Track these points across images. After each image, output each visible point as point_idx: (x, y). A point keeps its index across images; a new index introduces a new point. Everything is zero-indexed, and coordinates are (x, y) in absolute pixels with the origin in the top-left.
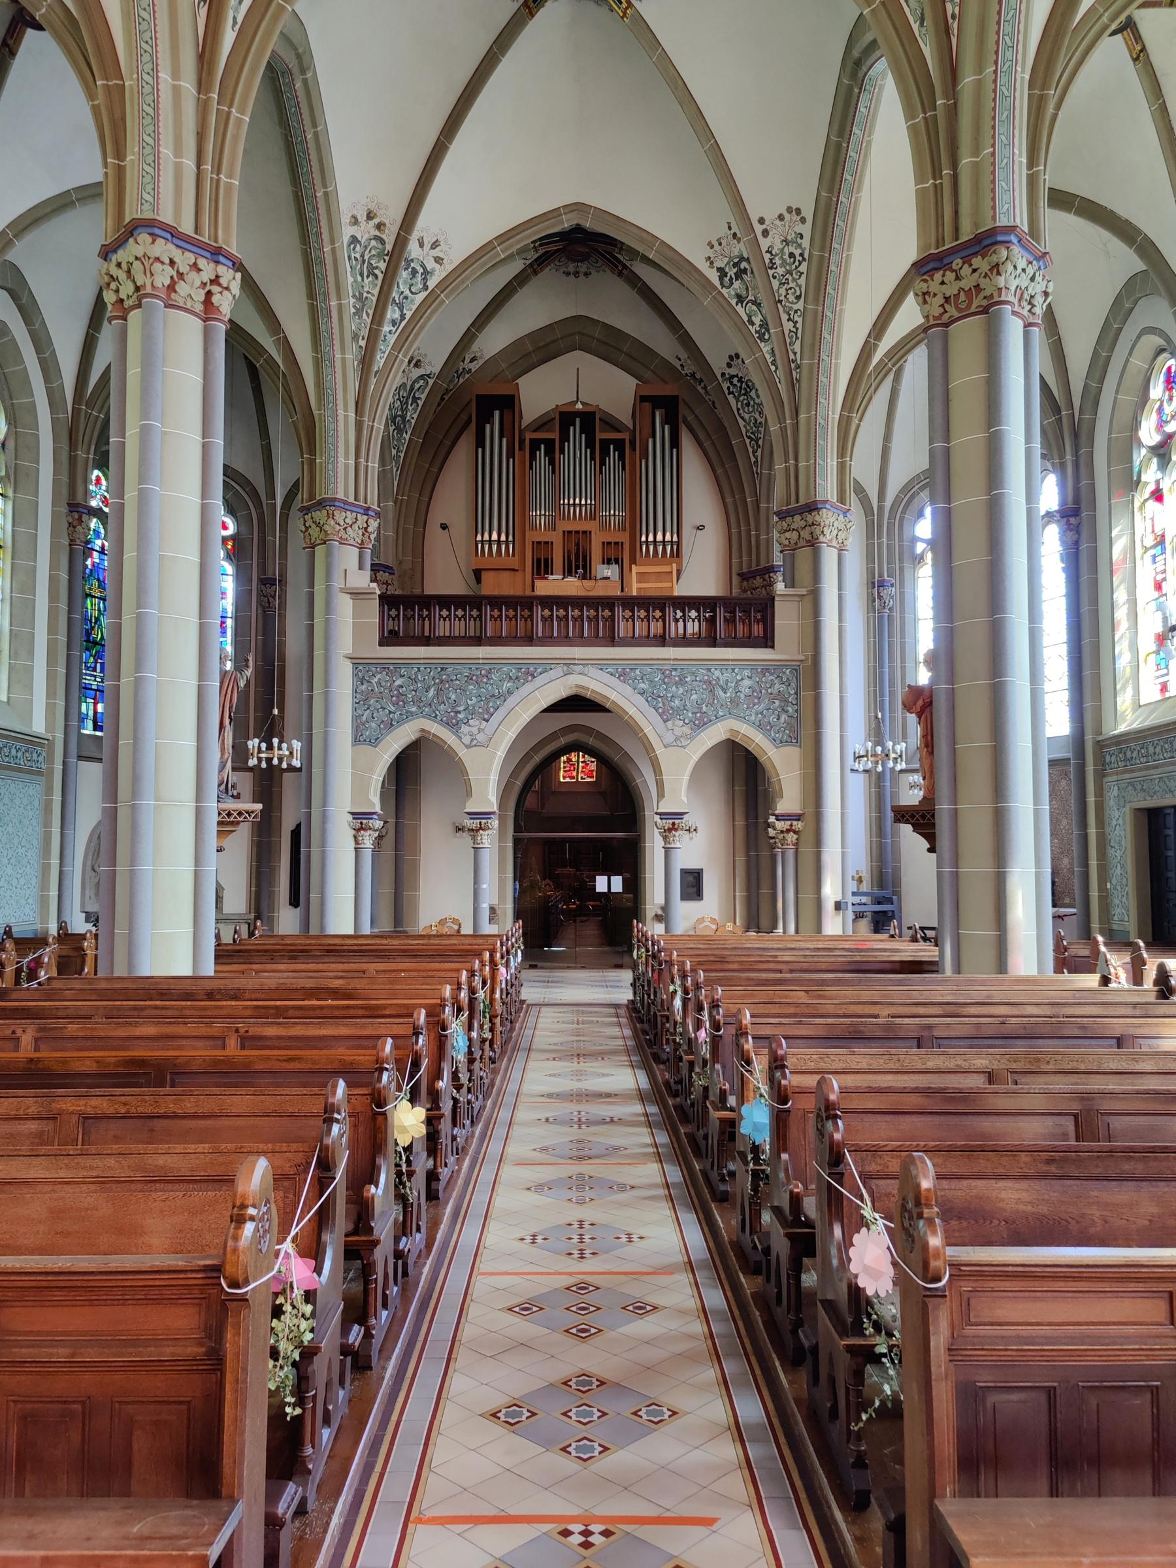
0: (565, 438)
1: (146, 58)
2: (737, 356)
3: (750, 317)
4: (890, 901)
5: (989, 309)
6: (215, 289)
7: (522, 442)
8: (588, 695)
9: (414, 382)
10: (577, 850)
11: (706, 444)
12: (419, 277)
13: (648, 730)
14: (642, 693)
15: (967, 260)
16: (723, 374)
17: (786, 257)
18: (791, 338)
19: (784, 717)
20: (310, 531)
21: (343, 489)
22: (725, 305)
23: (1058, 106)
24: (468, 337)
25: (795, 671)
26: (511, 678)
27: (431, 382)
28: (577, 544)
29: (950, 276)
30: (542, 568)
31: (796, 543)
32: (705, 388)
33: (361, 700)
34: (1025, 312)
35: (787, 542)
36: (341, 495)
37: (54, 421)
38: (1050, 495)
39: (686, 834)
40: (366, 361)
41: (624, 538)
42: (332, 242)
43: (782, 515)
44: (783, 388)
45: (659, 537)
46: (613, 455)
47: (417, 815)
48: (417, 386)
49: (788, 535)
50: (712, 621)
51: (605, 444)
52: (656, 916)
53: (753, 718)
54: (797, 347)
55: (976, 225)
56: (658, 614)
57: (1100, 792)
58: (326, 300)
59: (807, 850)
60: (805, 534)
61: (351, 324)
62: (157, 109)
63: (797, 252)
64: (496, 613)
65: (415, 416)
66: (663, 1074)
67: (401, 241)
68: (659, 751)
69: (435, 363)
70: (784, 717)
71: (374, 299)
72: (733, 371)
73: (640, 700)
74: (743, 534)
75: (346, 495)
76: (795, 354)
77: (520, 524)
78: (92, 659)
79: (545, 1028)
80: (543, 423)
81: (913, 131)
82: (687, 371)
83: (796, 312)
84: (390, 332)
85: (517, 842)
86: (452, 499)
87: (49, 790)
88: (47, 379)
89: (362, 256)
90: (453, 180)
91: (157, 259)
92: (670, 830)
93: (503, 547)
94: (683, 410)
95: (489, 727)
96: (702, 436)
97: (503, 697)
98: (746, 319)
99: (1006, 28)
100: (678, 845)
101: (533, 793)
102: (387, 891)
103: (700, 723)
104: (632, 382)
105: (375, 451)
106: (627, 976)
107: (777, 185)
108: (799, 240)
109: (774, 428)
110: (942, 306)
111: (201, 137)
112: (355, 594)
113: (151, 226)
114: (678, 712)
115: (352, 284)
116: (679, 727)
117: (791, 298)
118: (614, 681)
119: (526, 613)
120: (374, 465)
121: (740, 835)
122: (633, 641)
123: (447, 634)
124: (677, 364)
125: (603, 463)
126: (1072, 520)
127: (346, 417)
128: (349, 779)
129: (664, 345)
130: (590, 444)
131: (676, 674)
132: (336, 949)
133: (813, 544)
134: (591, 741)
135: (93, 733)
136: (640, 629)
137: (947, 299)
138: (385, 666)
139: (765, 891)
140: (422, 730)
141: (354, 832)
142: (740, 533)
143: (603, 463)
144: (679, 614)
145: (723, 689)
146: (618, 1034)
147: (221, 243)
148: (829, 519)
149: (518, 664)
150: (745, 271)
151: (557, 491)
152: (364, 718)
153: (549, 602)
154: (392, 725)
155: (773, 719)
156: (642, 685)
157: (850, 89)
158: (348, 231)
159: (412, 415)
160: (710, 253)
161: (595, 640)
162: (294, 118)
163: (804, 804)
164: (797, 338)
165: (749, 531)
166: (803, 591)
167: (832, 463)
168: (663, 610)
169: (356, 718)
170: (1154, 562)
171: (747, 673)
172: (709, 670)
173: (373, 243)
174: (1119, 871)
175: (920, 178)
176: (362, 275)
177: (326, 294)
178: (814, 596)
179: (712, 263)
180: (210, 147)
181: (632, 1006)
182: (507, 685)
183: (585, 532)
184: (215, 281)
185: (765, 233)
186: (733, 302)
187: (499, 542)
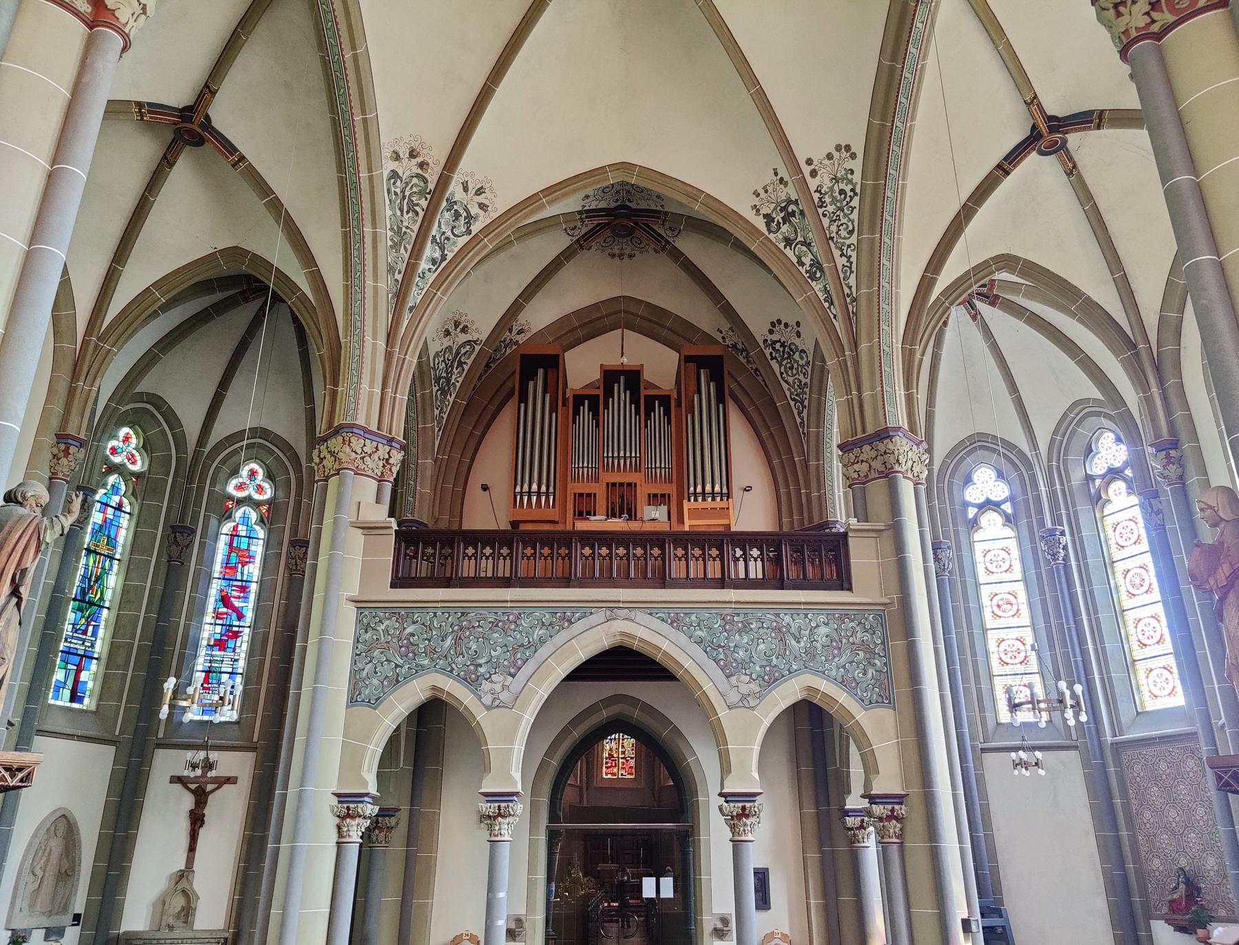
0: (609, 393)
2: (779, 322)
3: (799, 258)
5: (888, 475)
8: (636, 645)
9: (460, 347)
13: (707, 687)
14: (700, 642)
16: (765, 341)
17: (837, 194)
18: (845, 273)
20: (325, 462)
21: (364, 412)
22: (773, 248)
24: (516, 308)
25: (880, 617)
26: (543, 624)
27: (477, 348)
28: (622, 497)
31: (866, 476)
32: (747, 357)
33: (362, 651)
35: (856, 475)
36: (361, 421)
40: (401, 295)
44: (839, 325)
46: (658, 410)
47: (436, 801)
48: (463, 351)
49: (856, 467)
50: (778, 561)
52: (715, 929)
53: (834, 673)
54: (852, 281)
56: (714, 552)
58: (360, 225)
61: (386, 256)
63: (848, 188)
65: (461, 380)
67: (444, 181)
68: (722, 713)
69: (483, 328)
70: (871, 671)
71: (414, 235)
72: (775, 337)
73: (697, 651)
74: (792, 493)
76: (850, 288)
78: (83, 621)
83: (849, 246)
84: (429, 270)
85: (552, 836)
86: (495, 460)
89: (403, 191)
90: (492, 93)
92: (739, 816)
93: (543, 498)
94: (727, 366)
96: (745, 401)
97: (534, 647)
98: (795, 260)
100: (750, 837)
103: (770, 680)
105: (405, 384)
107: (825, 121)
108: (850, 176)
110: (1147, 14)
112: (369, 529)
114: (743, 665)
115: (388, 217)
116: (747, 685)
117: (843, 233)
118: (666, 628)
119: (563, 551)
120: (403, 397)
121: (811, 825)
123: (472, 575)
124: (719, 337)
125: (648, 417)
126: (1173, 453)
127: (374, 345)
129: (703, 317)
130: (635, 400)
135: (68, 704)
136: (695, 569)
139: (846, 898)
140: (434, 688)
141: (337, 820)
142: (789, 494)
143: (648, 417)
144: (739, 553)
145: (795, 638)
150: (793, 214)
152: (364, 673)
154: (398, 682)
155: (858, 674)
156: (699, 633)
160: (757, 201)
161: (643, 581)
162: (330, 34)
164: (852, 272)
168: (720, 549)
169: (354, 673)
171: (822, 618)
172: (778, 615)
173: (415, 180)
176: (401, 210)
177: (360, 221)
179: (758, 211)
182: (539, 632)
183: (629, 484)
185: (814, 174)
186: (781, 246)
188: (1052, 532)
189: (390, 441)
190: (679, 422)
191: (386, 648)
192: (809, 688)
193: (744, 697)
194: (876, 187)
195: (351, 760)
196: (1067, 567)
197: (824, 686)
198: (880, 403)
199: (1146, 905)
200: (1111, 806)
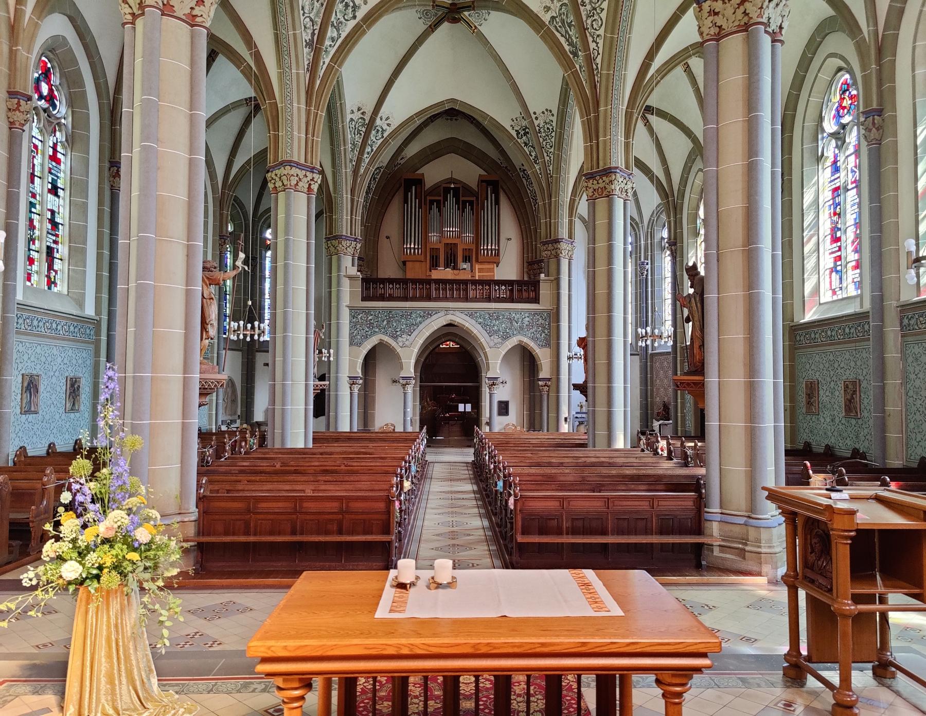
0: (446, 199)
5: (609, 196)
10: (450, 378)
13: (482, 340)
21: (345, 230)
24: (400, 150)
25: (549, 315)
29: (595, 182)
30: (434, 265)
33: (353, 325)
36: (344, 233)
39: (501, 384)
40: (356, 172)
41: (473, 247)
43: (544, 243)
50: (512, 291)
51: (464, 202)
54: (599, 60)
55: (605, 164)
58: (339, 145)
59: (552, 394)
61: (349, 156)
66: (482, 485)
79: (437, 471)
80: (436, 187)
86: (391, 224)
95: (411, 338)
97: (417, 325)
99: (615, 92)
103: (506, 337)
106: (472, 450)
112: (351, 278)
113: (290, 163)
115: (351, 137)
116: (496, 339)
118: (467, 318)
121: (527, 385)
122: (475, 300)
125: (463, 211)
128: (349, 362)
130: (457, 202)
131: (495, 316)
132: (348, 438)
133: (557, 257)
138: (367, 311)
146: (466, 473)
149: (424, 310)
153: (438, 282)
155: (538, 336)
163: (552, 374)
166: (552, 278)
169: (351, 334)
175: (585, 142)
178: (558, 281)
180: (311, 128)
181: (473, 463)
182: (419, 319)
184: (312, 180)
185: (537, 118)
187: (414, 248)
188: (643, 264)
190: (477, 213)
191: (362, 324)
195: (352, 365)
196: (647, 279)
198: (607, 150)
199: (652, 414)
200: (646, 377)
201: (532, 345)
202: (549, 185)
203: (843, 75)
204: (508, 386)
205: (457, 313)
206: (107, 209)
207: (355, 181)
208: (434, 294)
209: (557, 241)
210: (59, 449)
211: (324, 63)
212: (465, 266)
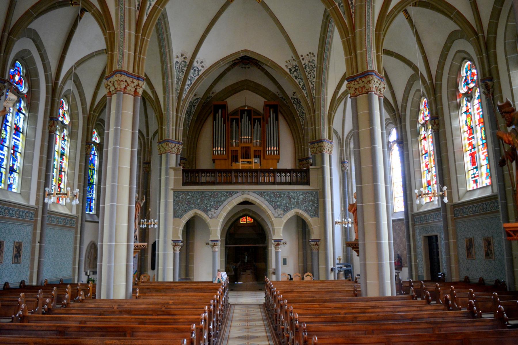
1: (122, 26)
4: (350, 266)
5: (368, 92)
6: (138, 87)
7: (228, 118)
10: (247, 251)
11: (287, 119)
12: (197, 72)
13: (269, 212)
14: (267, 200)
15: (360, 79)
19: (313, 208)
23: (384, 36)
29: (356, 83)
30: (235, 159)
34: (378, 93)
36: (171, 138)
37: (83, 117)
38: (394, 136)
40: (179, 97)
42: (170, 63)
43: (312, 143)
45: (272, 149)
51: (255, 120)
54: (314, 92)
55: (363, 69)
57: (414, 231)
58: (168, 79)
60: (318, 149)
61: (175, 86)
62: (124, 40)
63: (313, 65)
64: (220, 175)
67: (191, 62)
68: (273, 219)
70: (313, 208)
72: (295, 97)
73: (267, 203)
75: (172, 138)
77: (227, 145)
79: (236, 313)
80: (235, 112)
81: (343, 42)
82: (280, 96)
87: (76, 233)
88: (82, 105)
91: (122, 81)
92: (277, 245)
97: (222, 202)
101: (233, 232)
102: (184, 265)
103: (286, 210)
104: (263, 100)
107: (306, 46)
109: (308, 116)
111: (136, 45)
113: (120, 72)
116: (280, 211)
117: (312, 78)
118: (258, 196)
119: (230, 175)
120: (181, 128)
124: (277, 94)
125: (254, 125)
126: (436, 120)
127: (173, 114)
129: (272, 88)
130: (250, 119)
133: (321, 153)
134: (251, 214)
136: (266, 179)
137: (356, 89)
138: (187, 193)
147: (140, 75)
148: (326, 145)
150: (297, 70)
151: (239, 134)
153: (237, 171)
155: (310, 208)
157: (326, 23)
158: (175, 60)
159: (193, 111)
165: (301, 146)
167: (326, 127)
170: (425, 159)
171: (301, 193)
173: (183, 63)
174: (420, 256)
175: (346, 55)
180: (138, 48)
182: (223, 198)
183: (248, 147)
184: (138, 85)
186: (294, 78)
187: (221, 150)
189: (179, 143)
192: (296, 212)
193: (279, 215)
194: (320, 67)
195: (175, 231)
197: (301, 212)
201: (305, 215)
202: (313, 103)
203: (466, 62)
204: (287, 246)
205: (251, 193)
206: (46, 144)
207: (179, 103)
208: (234, 180)
209: (321, 141)
210: (11, 286)
211: (150, 5)
212: (256, 161)
